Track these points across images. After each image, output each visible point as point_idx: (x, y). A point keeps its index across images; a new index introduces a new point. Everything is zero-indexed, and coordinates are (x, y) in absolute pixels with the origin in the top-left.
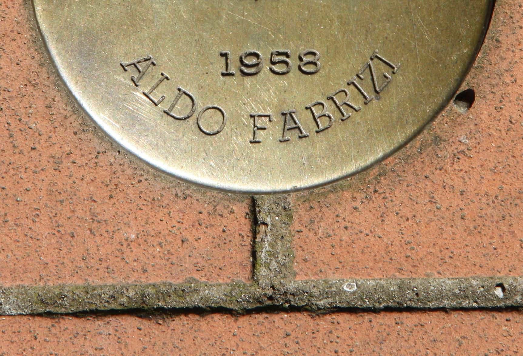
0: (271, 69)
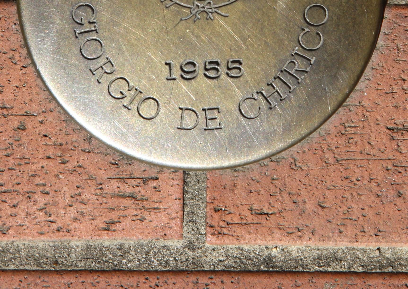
0: (205, 75)
